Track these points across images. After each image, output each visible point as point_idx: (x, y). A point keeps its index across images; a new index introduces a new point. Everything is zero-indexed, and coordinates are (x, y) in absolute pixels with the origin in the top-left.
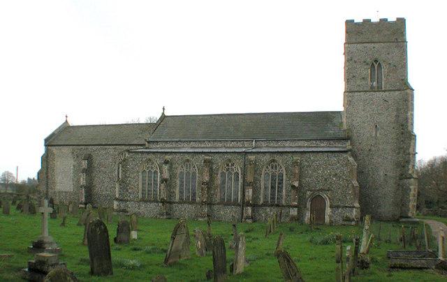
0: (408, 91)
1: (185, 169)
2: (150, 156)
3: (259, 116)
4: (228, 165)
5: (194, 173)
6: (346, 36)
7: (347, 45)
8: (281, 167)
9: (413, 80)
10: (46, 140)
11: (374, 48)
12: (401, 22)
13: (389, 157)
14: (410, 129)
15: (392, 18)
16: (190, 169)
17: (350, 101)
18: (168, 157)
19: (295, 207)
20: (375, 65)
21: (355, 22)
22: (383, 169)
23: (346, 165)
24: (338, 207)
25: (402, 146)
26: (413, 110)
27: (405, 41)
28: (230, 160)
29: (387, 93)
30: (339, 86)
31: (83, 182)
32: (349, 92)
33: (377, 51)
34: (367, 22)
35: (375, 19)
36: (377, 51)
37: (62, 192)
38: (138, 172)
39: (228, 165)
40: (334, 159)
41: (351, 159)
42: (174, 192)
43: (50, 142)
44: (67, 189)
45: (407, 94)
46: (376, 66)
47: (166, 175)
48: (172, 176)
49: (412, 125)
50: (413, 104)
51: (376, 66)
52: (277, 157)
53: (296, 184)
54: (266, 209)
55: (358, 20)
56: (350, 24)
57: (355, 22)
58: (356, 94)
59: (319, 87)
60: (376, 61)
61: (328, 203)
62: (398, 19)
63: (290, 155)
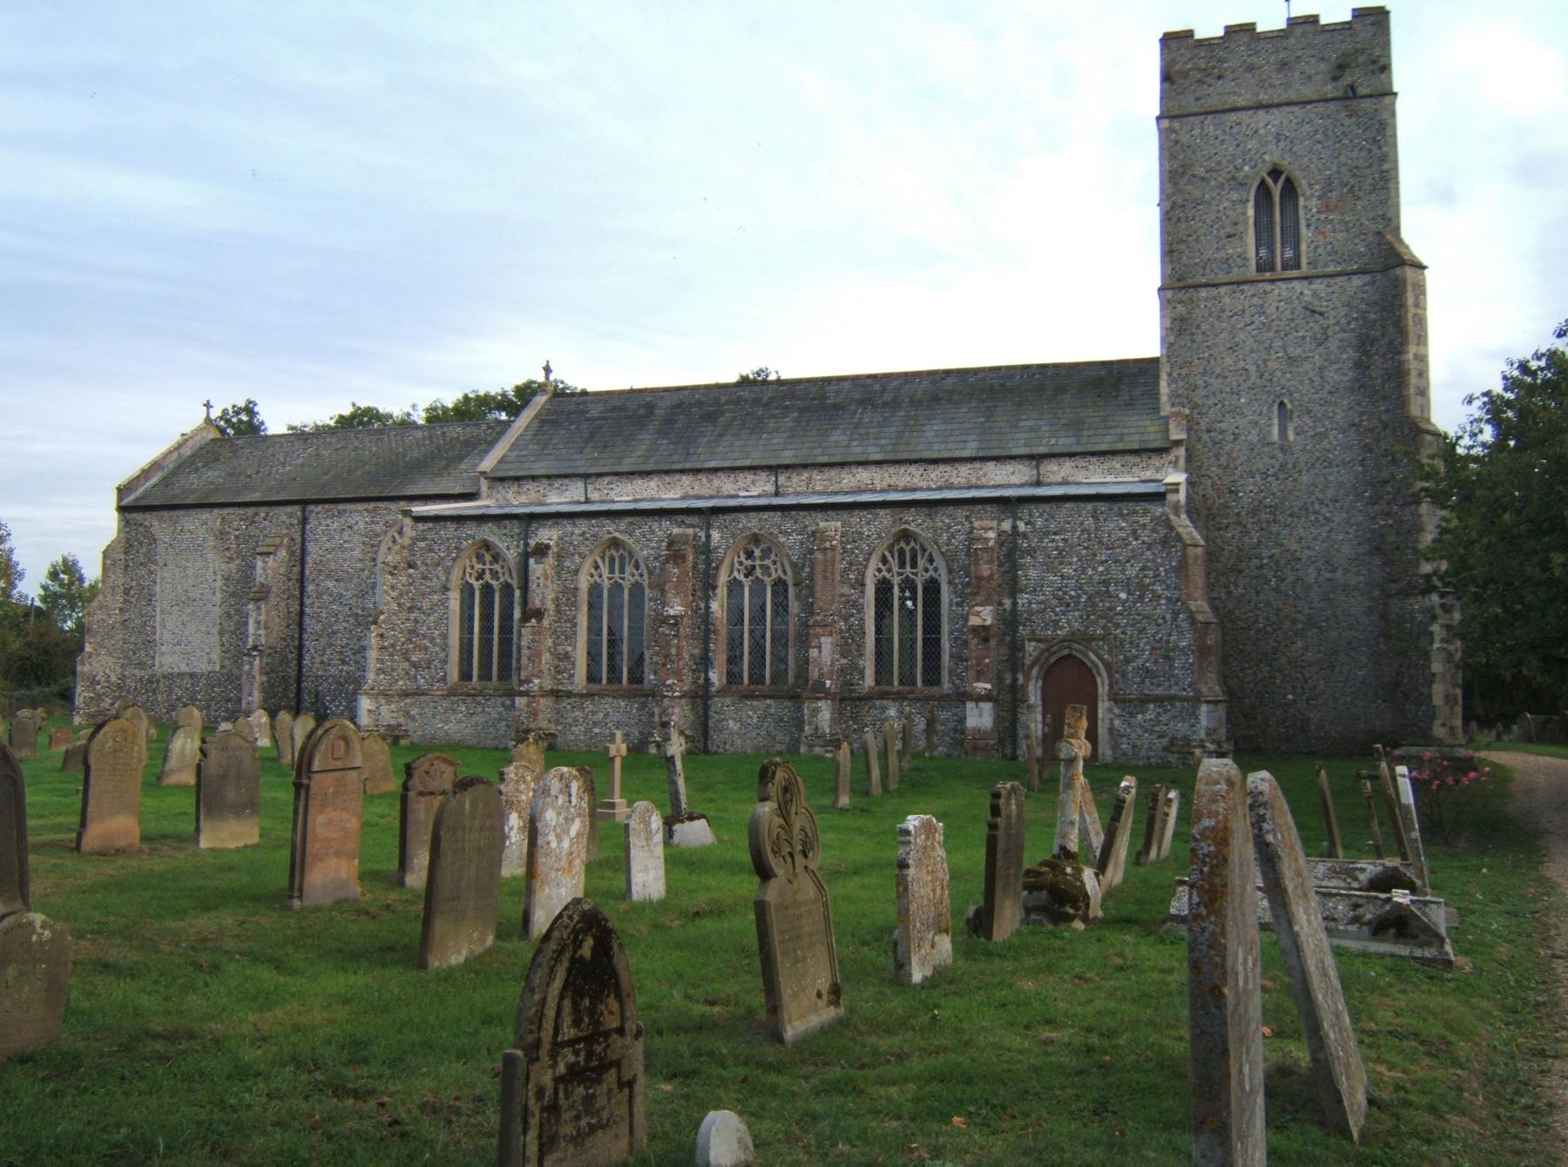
0: (1409, 273)
1: (606, 574)
2: (488, 532)
3: (846, 385)
4: (750, 555)
5: (932, 588)
6: (1163, 92)
7: (1166, 123)
8: (931, 560)
10: (122, 491)
11: (167, 999)
13: (1340, 517)
14: (1414, 411)
16: (622, 571)
17: (1183, 320)
19: (987, 697)
20: (1277, 193)
21: (1198, 36)
23: (1164, 542)
24: (1144, 701)
25: (1385, 474)
26: (1422, 339)
27: (1387, 93)
28: (756, 539)
29: (1319, 285)
33: (1281, 152)
34: (1241, 33)
35: (1271, 20)
36: (1281, 152)
37: (181, 675)
38: (446, 589)
39: (750, 555)
40: (1116, 525)
42: (567, 656)
44: (203, 667)
45: (1397, 279)
46: (1276, 190)
51: (1276, 190)
52: (915, 522)
54: (884, 709)
55: (1209, 28)
56: (1187, 63)
57: (1198, 36)
58: (1203, 293)
59: (1078, 275)
60: (1275, 173)
62: (1359, 14)
63: (961, 513)
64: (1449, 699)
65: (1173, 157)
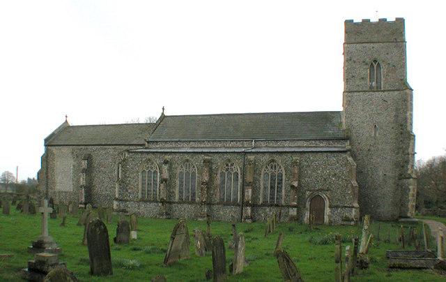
0: (407, 91)
1: (184, 169)
2: (150, 156)
3: (258, 116)
4: (227, 165)
6: (345, 36)
7: (346, 45)
8: (280, 167)
9: (412, 80)
10: (46, 140)
12: (400, 22)
13: (389, 157)
14: (409, 129)
15: (391, 18)
16: (189, 169)
17: (350, 101)
18: (168, 157)
19: (295, 207)
20: (374, 65)
21: (354, 22)
22: (382, 169)
23: (346, 165)
24: (337, 207)
25: (401, 146)
26: (412, 110)
27: (404, 41)
28: (229, 160)
29: (386, 93)
30: (339, 86)
31: (82, 182)
32: (348, 92)
33: (376, 51)
34: (366, 22)
35: (374, 19)
36: (376, 51)
37: (62, 192)
38: (138, 172)
39: (227, 165)
40: (333, 159)
41: (350, 159)
42: (173, 192)
43: (50, 142)
44: (67, 189)
45: (406, 94)
46: (375, 66)
47: (166, 175)
48: (172, 176)
49: (411, 125)
50: (412, 104)
51: (375, 66)
52: (276, 157)
53: (296, 184)
54: (265, 209)
55: (358, 20)
56: (349, 24)
57: (354, 22)
58: (355, 94)
59: (318, 87)
60: (375, 61)
61: (327, 203)
62: (397, 19)
63: (289, 155)
64: (413, 206)
65: (406, 119)
